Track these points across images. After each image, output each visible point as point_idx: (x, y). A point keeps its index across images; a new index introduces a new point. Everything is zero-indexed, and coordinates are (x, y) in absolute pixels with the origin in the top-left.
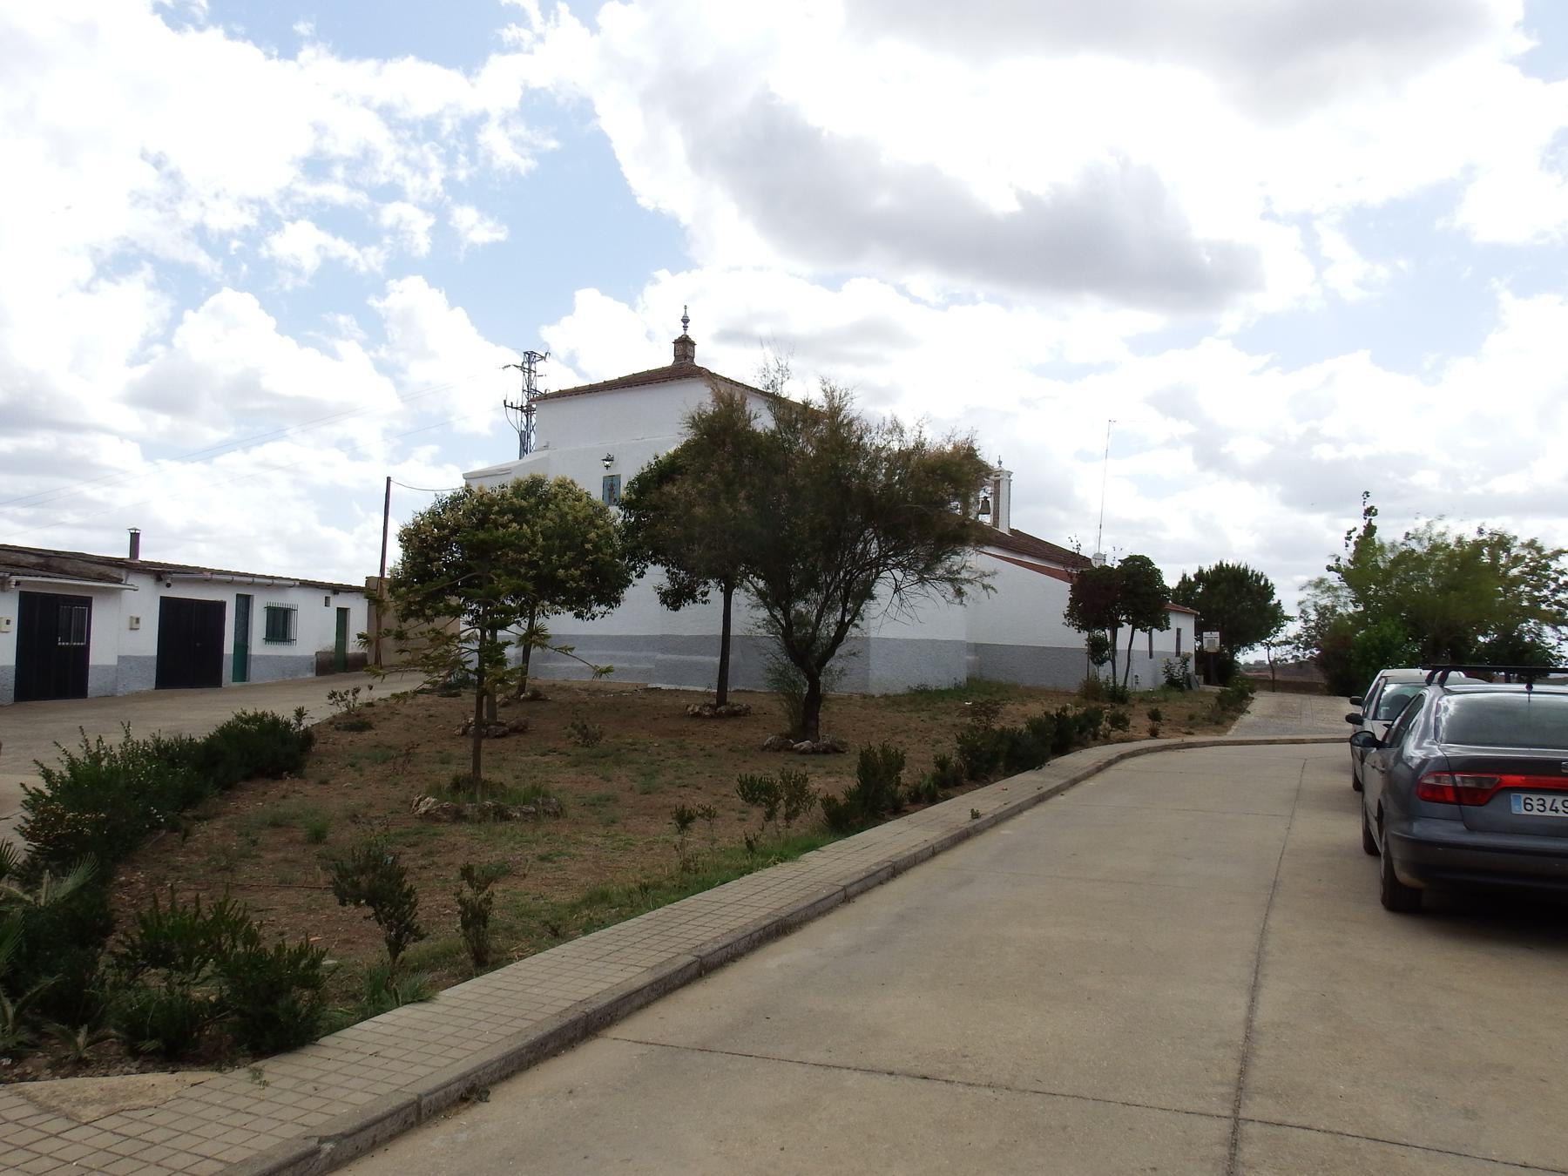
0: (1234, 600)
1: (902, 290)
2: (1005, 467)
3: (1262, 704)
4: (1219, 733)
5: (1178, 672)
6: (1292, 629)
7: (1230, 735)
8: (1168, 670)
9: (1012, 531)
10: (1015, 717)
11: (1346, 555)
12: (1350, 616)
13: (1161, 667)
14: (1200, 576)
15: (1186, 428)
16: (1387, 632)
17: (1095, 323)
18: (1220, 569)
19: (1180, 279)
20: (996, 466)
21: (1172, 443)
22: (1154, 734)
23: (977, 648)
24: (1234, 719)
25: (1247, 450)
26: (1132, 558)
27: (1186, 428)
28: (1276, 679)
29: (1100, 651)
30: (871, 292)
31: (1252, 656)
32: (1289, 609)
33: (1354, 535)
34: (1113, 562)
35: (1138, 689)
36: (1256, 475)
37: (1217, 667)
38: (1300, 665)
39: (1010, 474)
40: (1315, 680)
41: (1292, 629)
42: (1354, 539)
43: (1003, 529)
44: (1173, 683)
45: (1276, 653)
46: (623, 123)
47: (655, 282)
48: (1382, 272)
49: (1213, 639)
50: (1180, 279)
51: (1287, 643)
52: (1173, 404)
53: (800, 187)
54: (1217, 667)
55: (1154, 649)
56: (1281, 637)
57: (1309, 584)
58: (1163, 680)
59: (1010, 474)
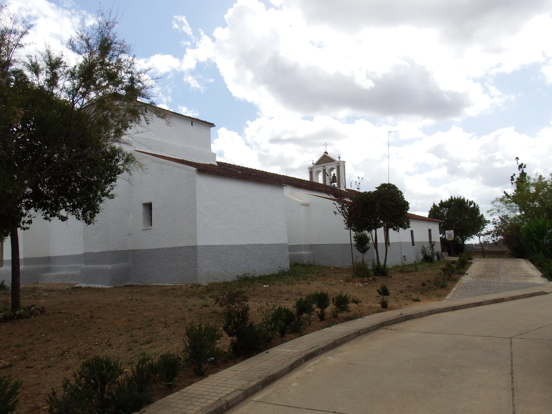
0: (457, 215)
1: (335, 118)
2: (342, 159)
3: (477, 266)
4: (440, 297)
5: (429, 252)
6: (490, 227)
7: (449, 300)
8: (424, 251)
9: (348, 190)
10: (258, 309)
11: (511, 190)
12: (519, 217)
13: (420, 249)
14: (442, 204)
15: (444, 160)
16: (541, 222)
17: (410, 125)
18: (451, 200)
19: (440, 106)
20: (337, 159)
21: (439, 166)
22: (385, 306)
23: (292, 248)
24: (456, 281)
25: (468, 166)
26: (384, 186)
27: (444, 160)
28: (484, 251)
29: (362, 244)
30: (323, 121)
31: (473, 241)
32: (487, 217)
33: (515, 178)
34: (373, 189)
35: (406, 263)
36: (472, 175)
37: (454, 247)
38: (495, 244)
39: (344, 162)
40: (505, 250)
41: (490, 227)
42: (515, 180)
43: (342, 189)
44: (428, 259)
45: (482, 239)
46: (228, 69)
47: (247, 126)
48: (513, 98)
49: (450, 234)
50: (440, 106)
51: (488, 233)
52: (438, 151)
53: (301, 91)
54: (454, 247)
55: (415, 240)
56: (484, 231)
57: (497, 199)
58: (421, 257)
59: (344, 162)
